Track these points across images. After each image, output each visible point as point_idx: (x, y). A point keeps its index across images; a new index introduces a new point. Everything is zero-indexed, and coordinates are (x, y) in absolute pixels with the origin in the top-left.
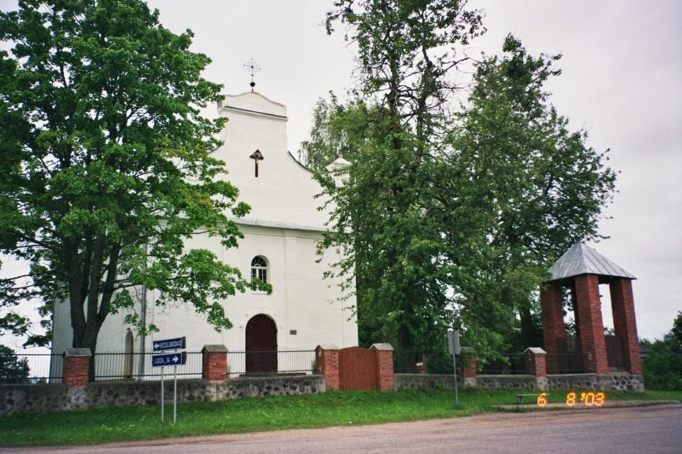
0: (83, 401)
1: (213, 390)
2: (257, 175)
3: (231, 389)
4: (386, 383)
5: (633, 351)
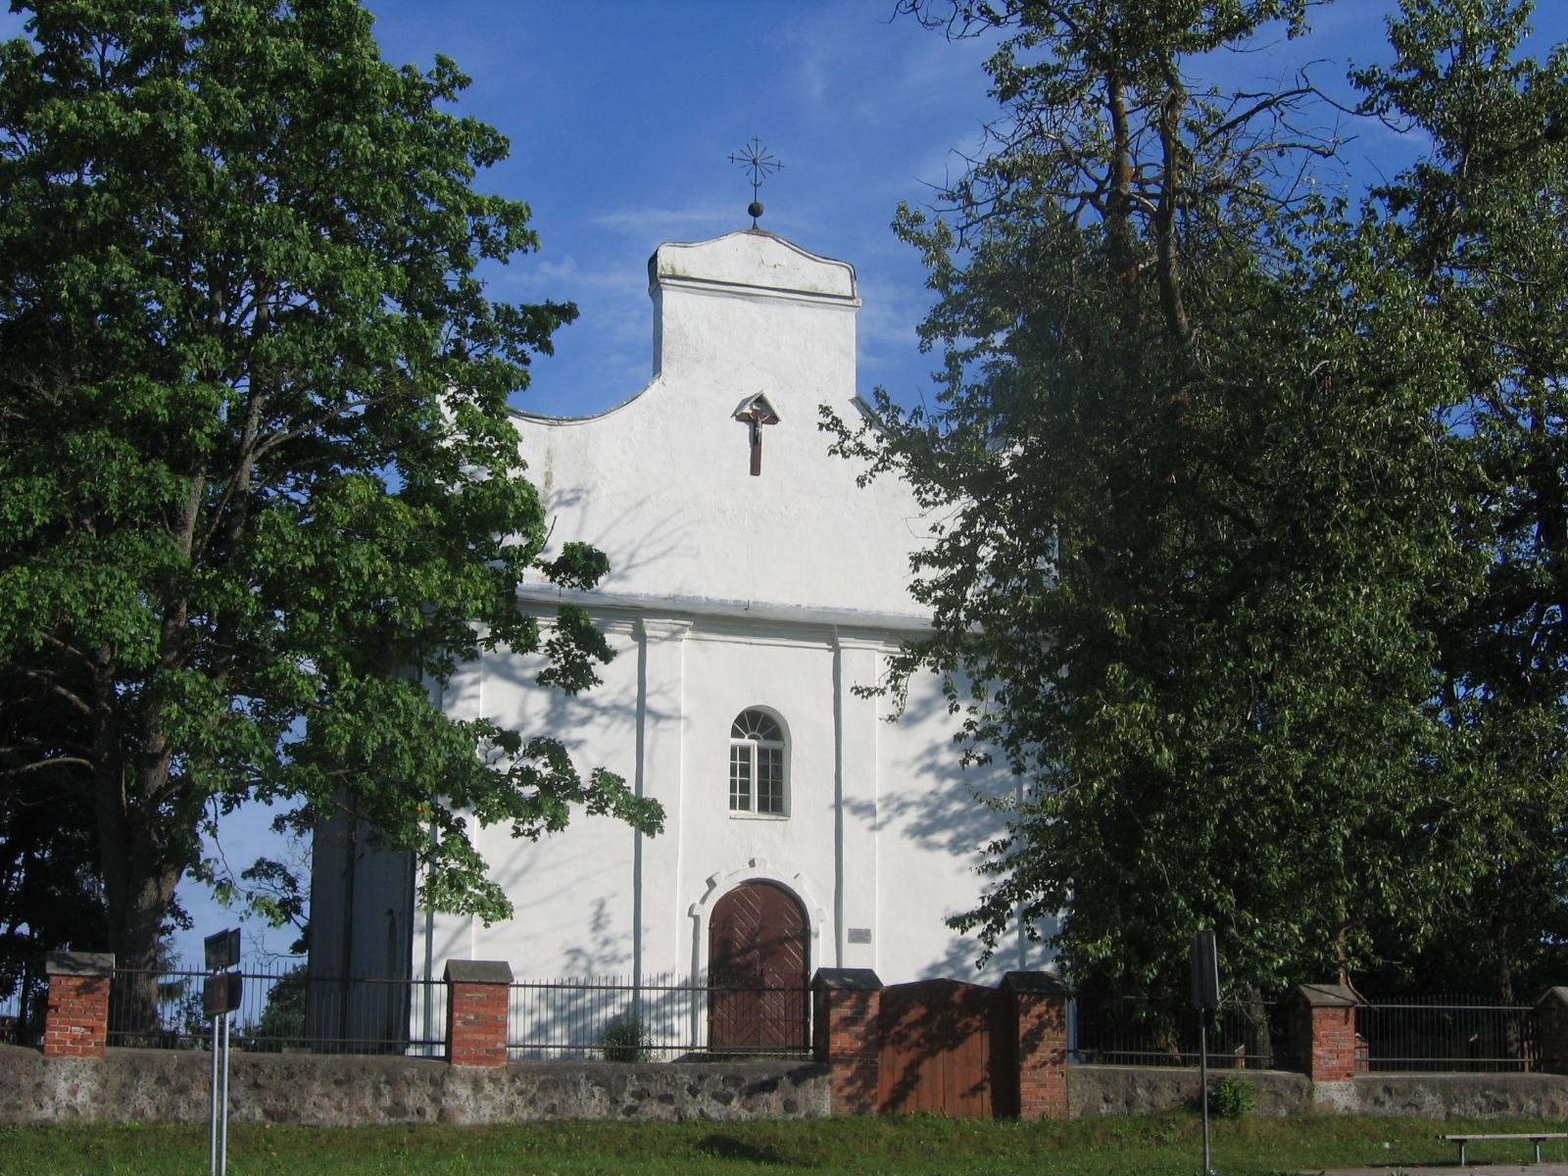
0: (87, 1098)
1: (464, 1091)
2: (755, 470)
3: (521, 1093)
4: (1042, 1092)
5: (1320, 1057)
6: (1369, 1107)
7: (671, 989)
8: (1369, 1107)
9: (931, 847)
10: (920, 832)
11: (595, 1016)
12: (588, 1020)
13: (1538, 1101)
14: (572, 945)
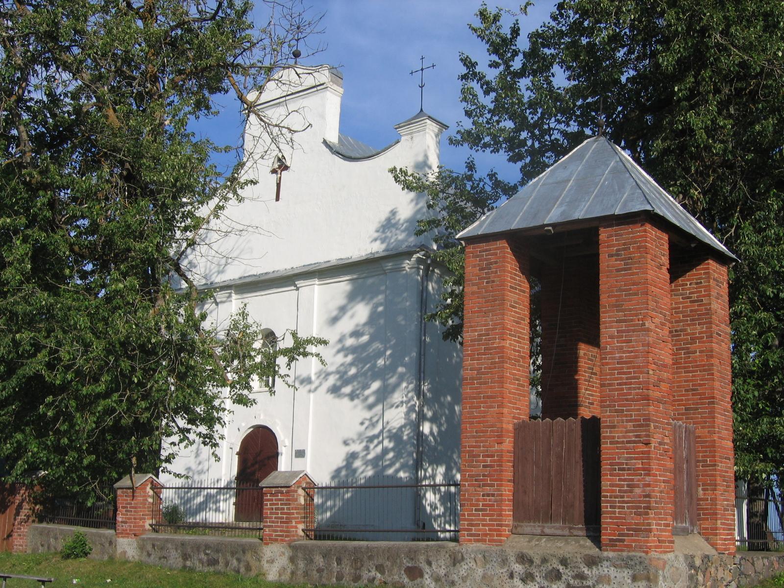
2: (277, 199)
6: (144, 558)
7: (220, 488)
8: (144, 558)
9: (340, 396)
10: (335, 390)
11: (195, 502)
12: (192, 503)
13: (239, 560)
14: (188, 466)
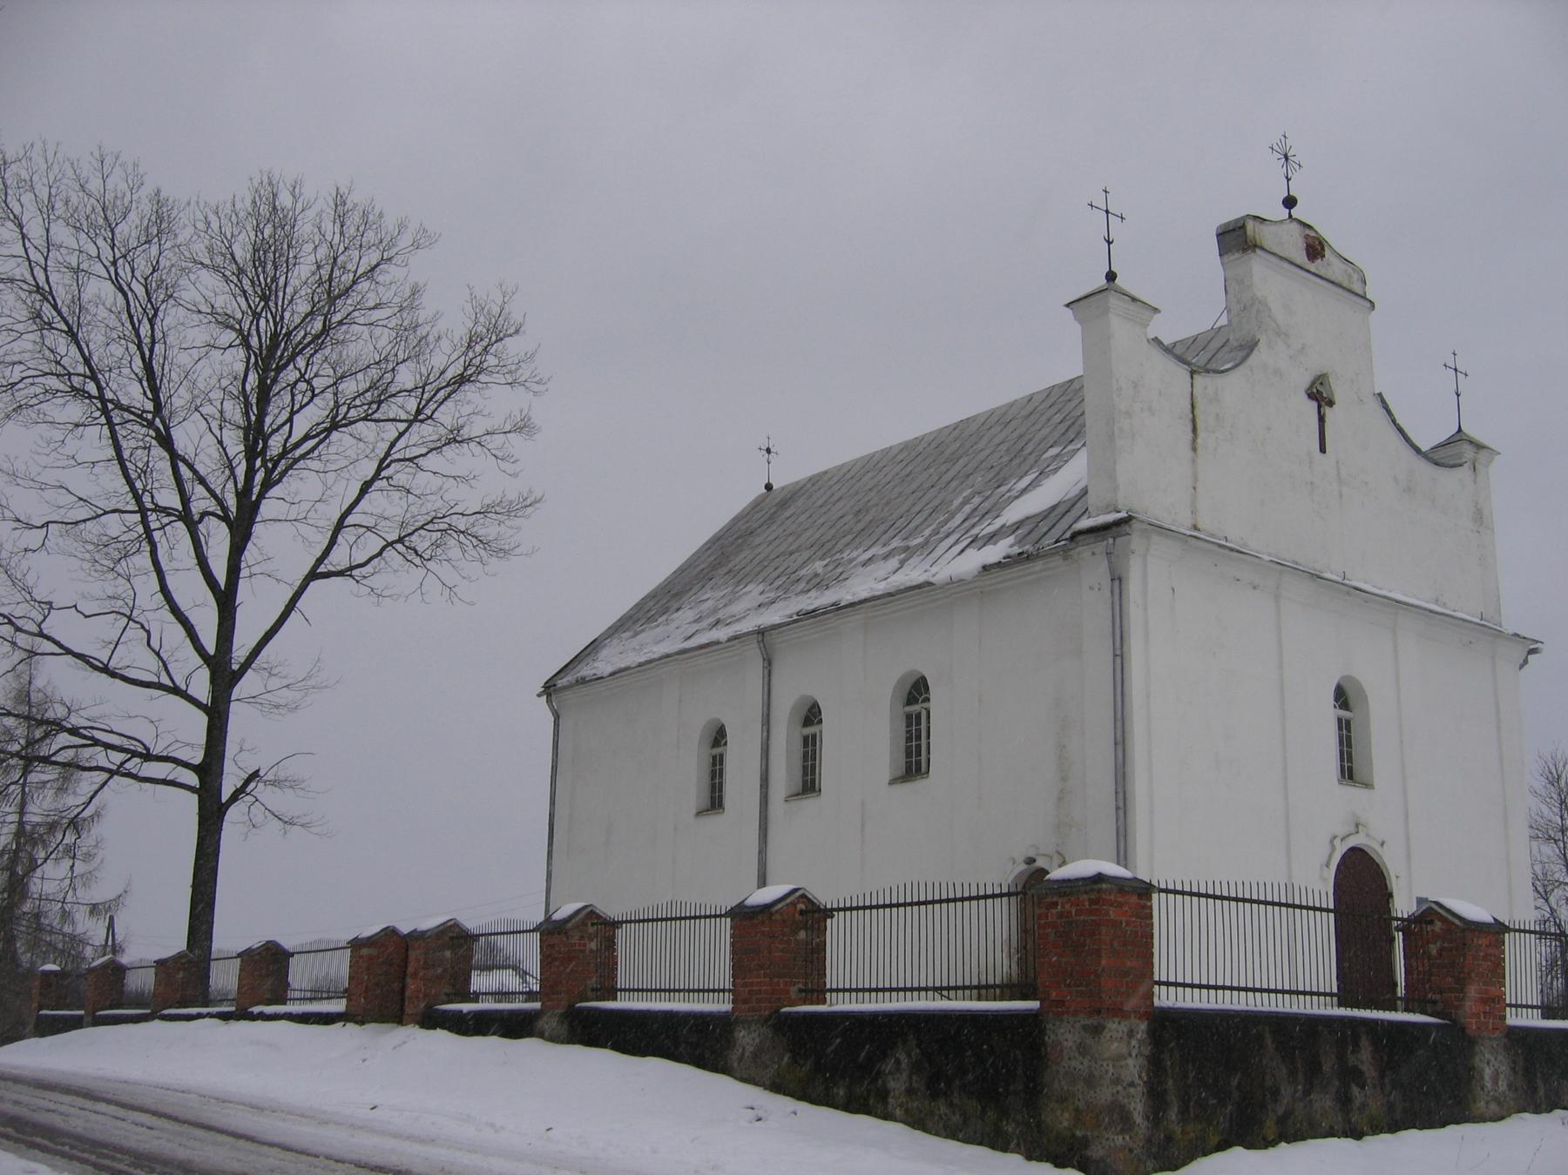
2: (1323, 449)
